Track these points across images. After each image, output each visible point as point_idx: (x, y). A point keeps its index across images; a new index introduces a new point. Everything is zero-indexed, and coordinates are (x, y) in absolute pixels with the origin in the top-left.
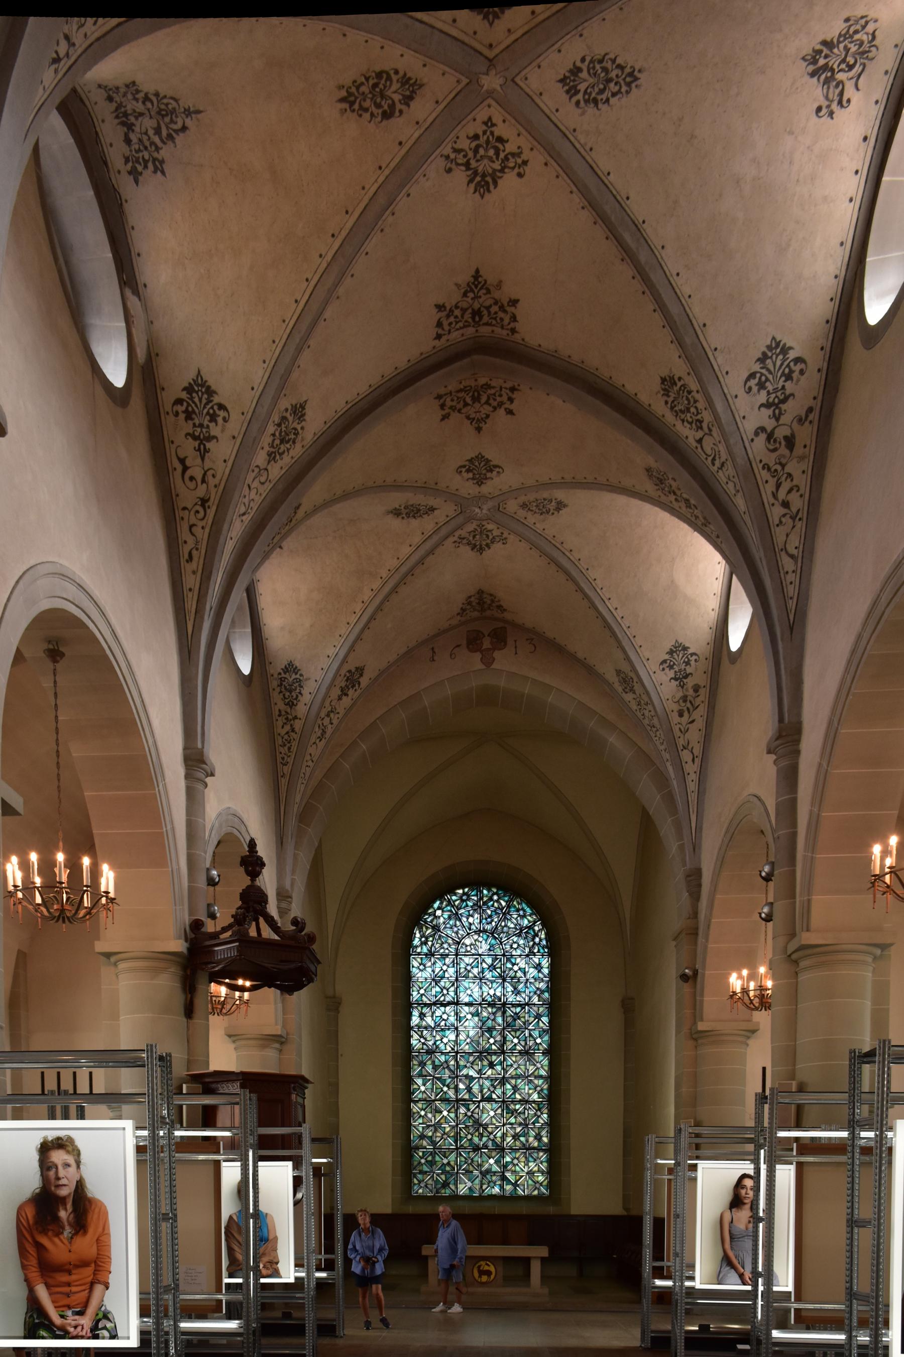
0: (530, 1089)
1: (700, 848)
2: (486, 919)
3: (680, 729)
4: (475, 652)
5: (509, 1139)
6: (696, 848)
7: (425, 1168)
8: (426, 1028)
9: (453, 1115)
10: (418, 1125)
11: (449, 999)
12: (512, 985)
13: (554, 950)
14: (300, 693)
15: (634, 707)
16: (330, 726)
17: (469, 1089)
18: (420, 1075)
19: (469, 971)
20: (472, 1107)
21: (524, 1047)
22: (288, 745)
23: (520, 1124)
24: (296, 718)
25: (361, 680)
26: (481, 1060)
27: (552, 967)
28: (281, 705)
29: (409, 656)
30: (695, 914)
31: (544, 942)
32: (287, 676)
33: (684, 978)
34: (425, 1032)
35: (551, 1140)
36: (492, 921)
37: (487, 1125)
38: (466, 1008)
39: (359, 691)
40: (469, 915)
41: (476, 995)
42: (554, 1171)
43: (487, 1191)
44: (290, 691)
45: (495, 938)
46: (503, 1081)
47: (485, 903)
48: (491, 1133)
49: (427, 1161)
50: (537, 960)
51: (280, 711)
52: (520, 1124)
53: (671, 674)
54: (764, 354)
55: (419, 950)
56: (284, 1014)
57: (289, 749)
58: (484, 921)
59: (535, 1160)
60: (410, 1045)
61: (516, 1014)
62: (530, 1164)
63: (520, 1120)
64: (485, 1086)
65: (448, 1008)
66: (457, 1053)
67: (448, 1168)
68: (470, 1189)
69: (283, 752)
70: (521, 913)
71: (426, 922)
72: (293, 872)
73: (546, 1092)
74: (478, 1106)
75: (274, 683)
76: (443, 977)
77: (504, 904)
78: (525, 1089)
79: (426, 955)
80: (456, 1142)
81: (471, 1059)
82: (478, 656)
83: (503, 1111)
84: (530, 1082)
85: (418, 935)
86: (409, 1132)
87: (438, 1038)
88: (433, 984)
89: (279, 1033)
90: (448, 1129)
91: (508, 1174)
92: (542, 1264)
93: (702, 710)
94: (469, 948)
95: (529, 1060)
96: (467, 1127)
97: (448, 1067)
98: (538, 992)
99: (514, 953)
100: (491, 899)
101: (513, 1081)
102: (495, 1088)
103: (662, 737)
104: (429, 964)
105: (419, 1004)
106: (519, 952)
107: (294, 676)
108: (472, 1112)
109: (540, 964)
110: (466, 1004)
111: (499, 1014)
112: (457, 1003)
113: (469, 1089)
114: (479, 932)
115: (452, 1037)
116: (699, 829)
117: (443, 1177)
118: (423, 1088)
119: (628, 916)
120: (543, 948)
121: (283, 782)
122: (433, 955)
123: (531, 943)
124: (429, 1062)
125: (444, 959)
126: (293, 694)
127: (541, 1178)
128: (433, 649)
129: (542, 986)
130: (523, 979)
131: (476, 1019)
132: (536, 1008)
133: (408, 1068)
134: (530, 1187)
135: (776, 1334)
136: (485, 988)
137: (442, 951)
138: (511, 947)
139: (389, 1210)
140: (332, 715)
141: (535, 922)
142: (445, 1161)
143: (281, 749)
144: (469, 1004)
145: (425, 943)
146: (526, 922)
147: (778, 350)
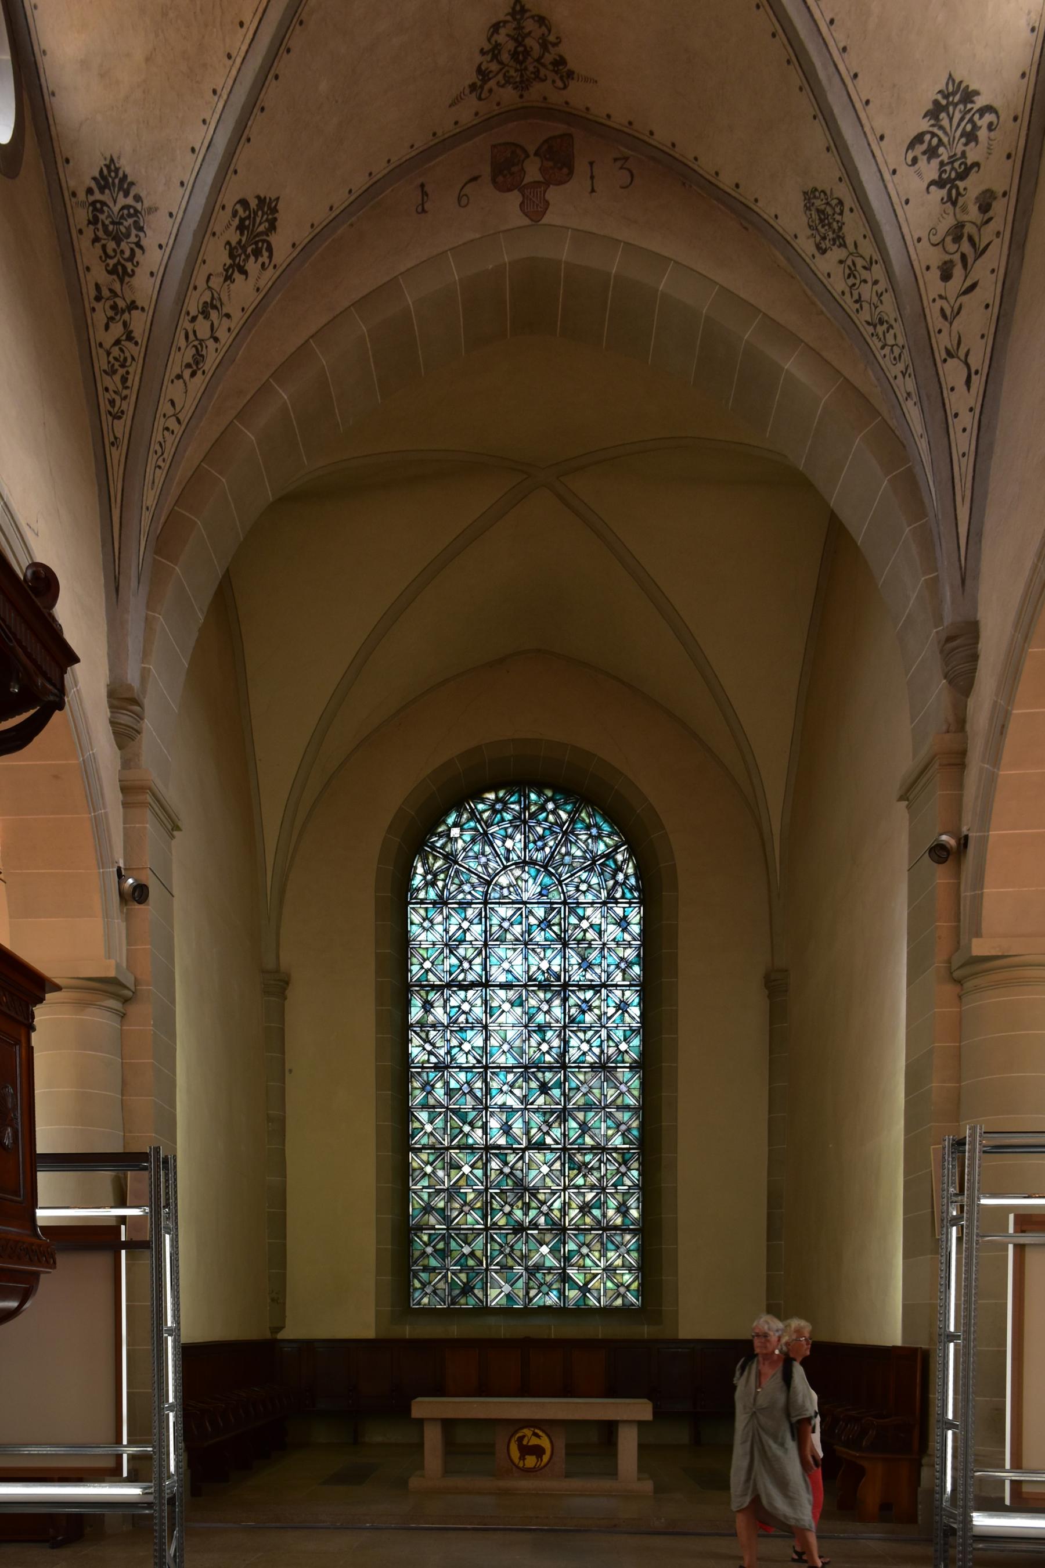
0: (608, 1128)
1: (976, 577)
2: (535, 842)
3: (942, 310)
4: (509, 190)
5: (573, 1213)
6: (967, 578)
7: (433, 1262)
8: (434, 1026)
9: (479, 1173)
10: (420, 1192)
11: (471, 977)
12: (578, 954)
13: (650, 893)
14: (138, 245)
15: (838, 284)
16: (211, 343)
17: (506, 1129)
18: (425, 1106)
19: (506, 931)
20: (512, 1159)
21: (599, 1057)
22: (122, 371)
23: (592, 1187)
24: (133, 306)
25: (273, 239)
26: (527, 1080)
27: (646, 922)
28: (99, 274)
29: (370, 200)
30: (960, 723)
31: (632, 881)
32: (106, 197)
33: (939, 853)
34: (432, 1034)
35: (644, 1214)
36: (545, 845)
37: (536, 1189)
38: (502, 993)
39: (270, 273)
40: (507, 836)
41: (519, 970)
42: (651, 1266)
43: (538, 1301)
44: (118, 240)
45: (550, 874)
46: (564, 1115)
47: (533, 816)
48: (543, 1203)
49: (436, 1251)
50: (619, 911)
51: (98, 287)
52: (592, 1187)
53: (930, 170)
54: (936, 102)
55: (422, 895)
56: (129, 944)
57: (124, 380)
58: (531, 846)
59: (618, 1248)
60: (408, 1055)
61: (585, 1001)
62: (610, 1254)
63: (592, 1179)
64: (533, 1124)
65: (470, 993)
66: (486, 1068)
67: (471, 1262)
68: (508, 1296)
69: (111, 387)
70: (594, 831)
71: (433, 848)
72: (145, 655)
73: (635, 1133)
74: (522, 1158)
75: (81, 216)
76: (462, 941)
77: (564, 816)
78: (602, 1128)
79: (434, 903)
80: (484, 1217)
81: (511, 1077)
82: (514, 198)
83: (563, 1165)
84: (609, 1116)
85: (420, 870)
86: (405, 1201)
87: (454, 1042)
88: (446, 951)
89: (112, 974)
90: (471, 1197)
91: (572, 1272)
92: (639, 1431)
93: (996, 256)
94: (505, 892)
95: (607, 1079)
96: (503, 1192)
97: (471, 1092)
98: (623, 965)
99: (582, 899)
100: (543, 808)
101: (580, 1115)
102: (550, 1126)
103: (901, 340)
104: (439, 919)
105: (422, 987)
106: (590, 898)
107: (122, 201)
108: (512, 1168)
109: (625, 917)
110: (502, 986)
111: (557, 1002)
112: (485, 984)
113: (506, 1129)
114: (523, 864)
115: (479, 1042)
116: (975, 534)
117: (463, 1276)
118: (429, 1128)
119: (776, 829)
120: (631, 891)
121: (116, 455)
122: (446, 904)
123: (611, 883)
124: (439, 1085)
125: (465, 909)
126: (124, 245)
127: (627, 1278)
128: (422, 186)
129: (630, 954)
130: (597, 944)
131: (518, 1010)
132: (618, 993)
133: (405, 1094)
134: (610, 1293)
135: (981, 1520)
136: (533, 960)
137: (461, 896)
138: (578, 890)
139: (370, 1334)
140: (214, 315)
141: (617, 847)
142: (466, 1250)
143: (107, 380)
144: (506, 986)
145: (433, 884)
146: (602, 847)
147: (957, 98)
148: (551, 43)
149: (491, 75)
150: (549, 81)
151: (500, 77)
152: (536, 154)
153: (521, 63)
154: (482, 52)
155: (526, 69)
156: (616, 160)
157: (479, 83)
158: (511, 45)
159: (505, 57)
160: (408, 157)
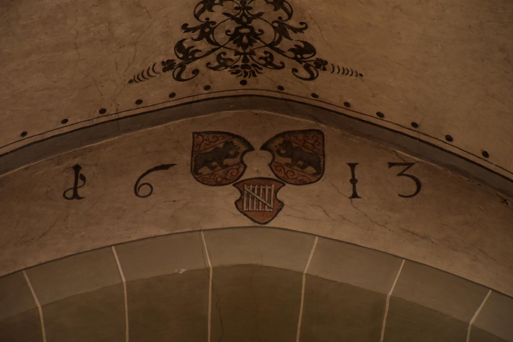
82: (228, 194)
148: (292, 28)
149: (197, 55)
150: (288, 70)
151: (212, 58)
152: (264, 147)
153: (245, 46)
154: (185, 27)
155: (252, 53)
156: (391, 165)
157: (178, 61)
158: (231, 26)
159: (220, 37)
160: (56, 133)
